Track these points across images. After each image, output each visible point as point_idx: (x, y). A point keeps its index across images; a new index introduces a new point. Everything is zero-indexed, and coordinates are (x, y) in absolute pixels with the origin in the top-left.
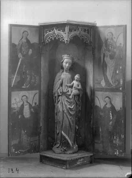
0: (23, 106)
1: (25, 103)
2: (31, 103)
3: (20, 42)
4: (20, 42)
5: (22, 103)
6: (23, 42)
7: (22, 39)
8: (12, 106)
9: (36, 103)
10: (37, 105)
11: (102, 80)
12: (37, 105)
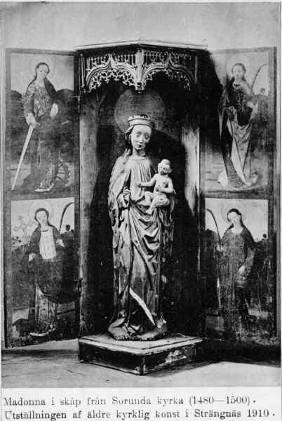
0: (38, 232)
1: (44, 227)
2: (58, 228)
3: (29, 89)
4: (29, 89)
5: (37, 226)
6: (37, 88)
7: (36, 82)
8: (14, 234)
9: (68, 227)
10: (70, 231)
11: (221, 172)
12: (70, 231)
